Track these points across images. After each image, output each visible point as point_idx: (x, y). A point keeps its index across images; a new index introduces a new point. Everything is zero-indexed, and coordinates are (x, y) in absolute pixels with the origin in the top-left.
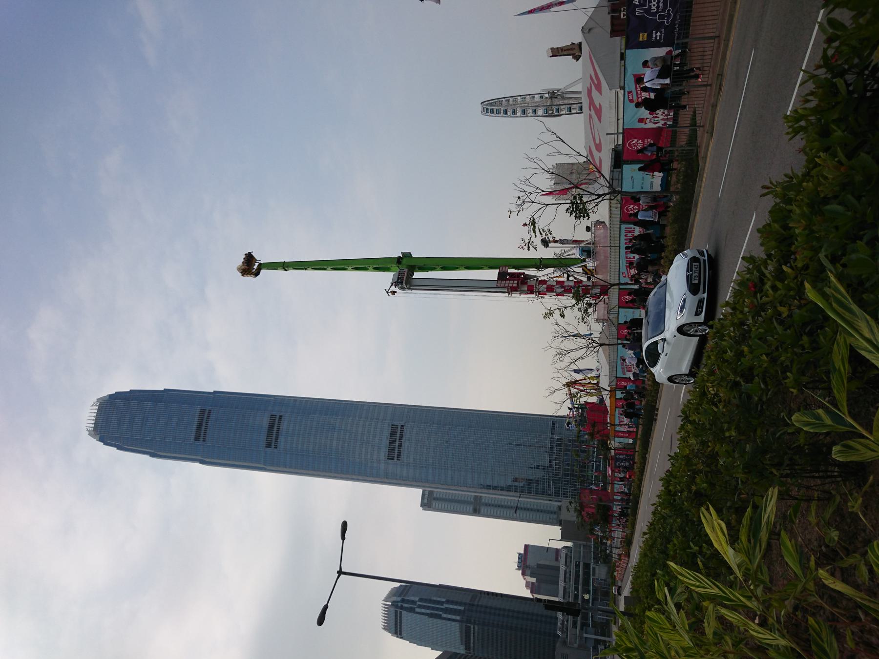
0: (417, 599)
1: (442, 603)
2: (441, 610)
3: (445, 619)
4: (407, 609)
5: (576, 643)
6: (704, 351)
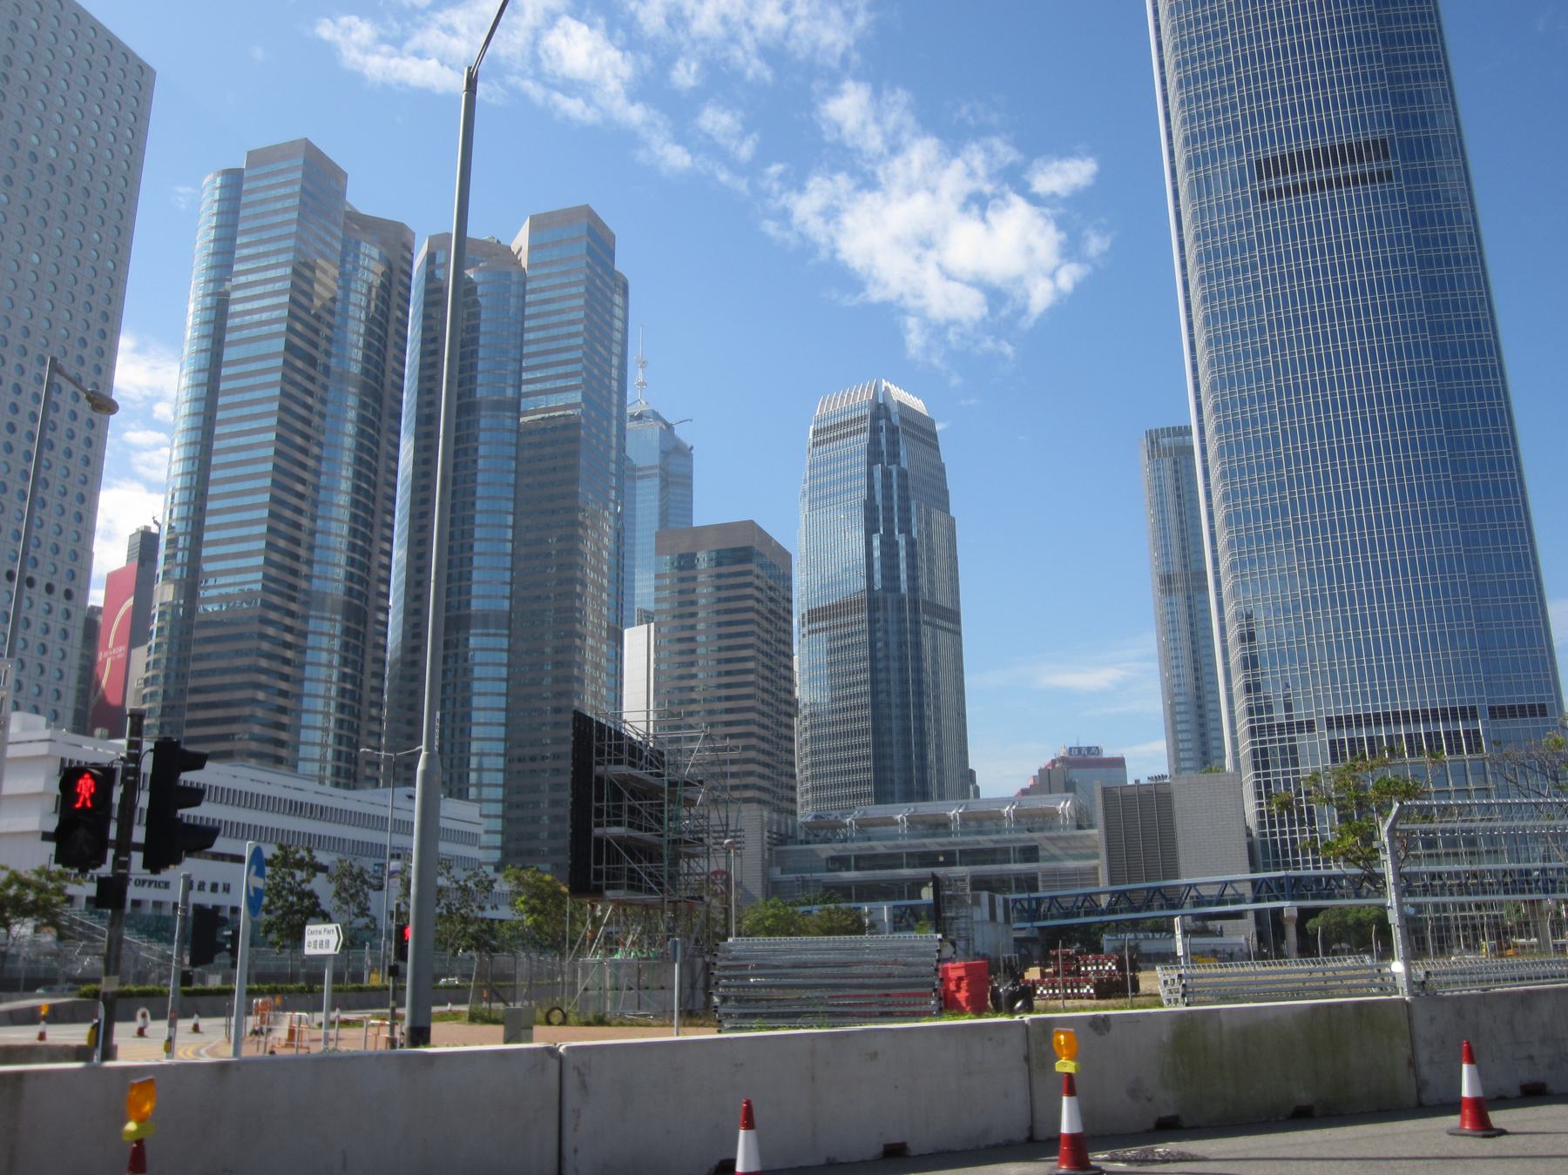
0: (904, 464)
1: (906, 529)
2: (889, 532)
3: (869, 544)
4: (874, 442)
5: (783, 872)
6: (196, 1016)
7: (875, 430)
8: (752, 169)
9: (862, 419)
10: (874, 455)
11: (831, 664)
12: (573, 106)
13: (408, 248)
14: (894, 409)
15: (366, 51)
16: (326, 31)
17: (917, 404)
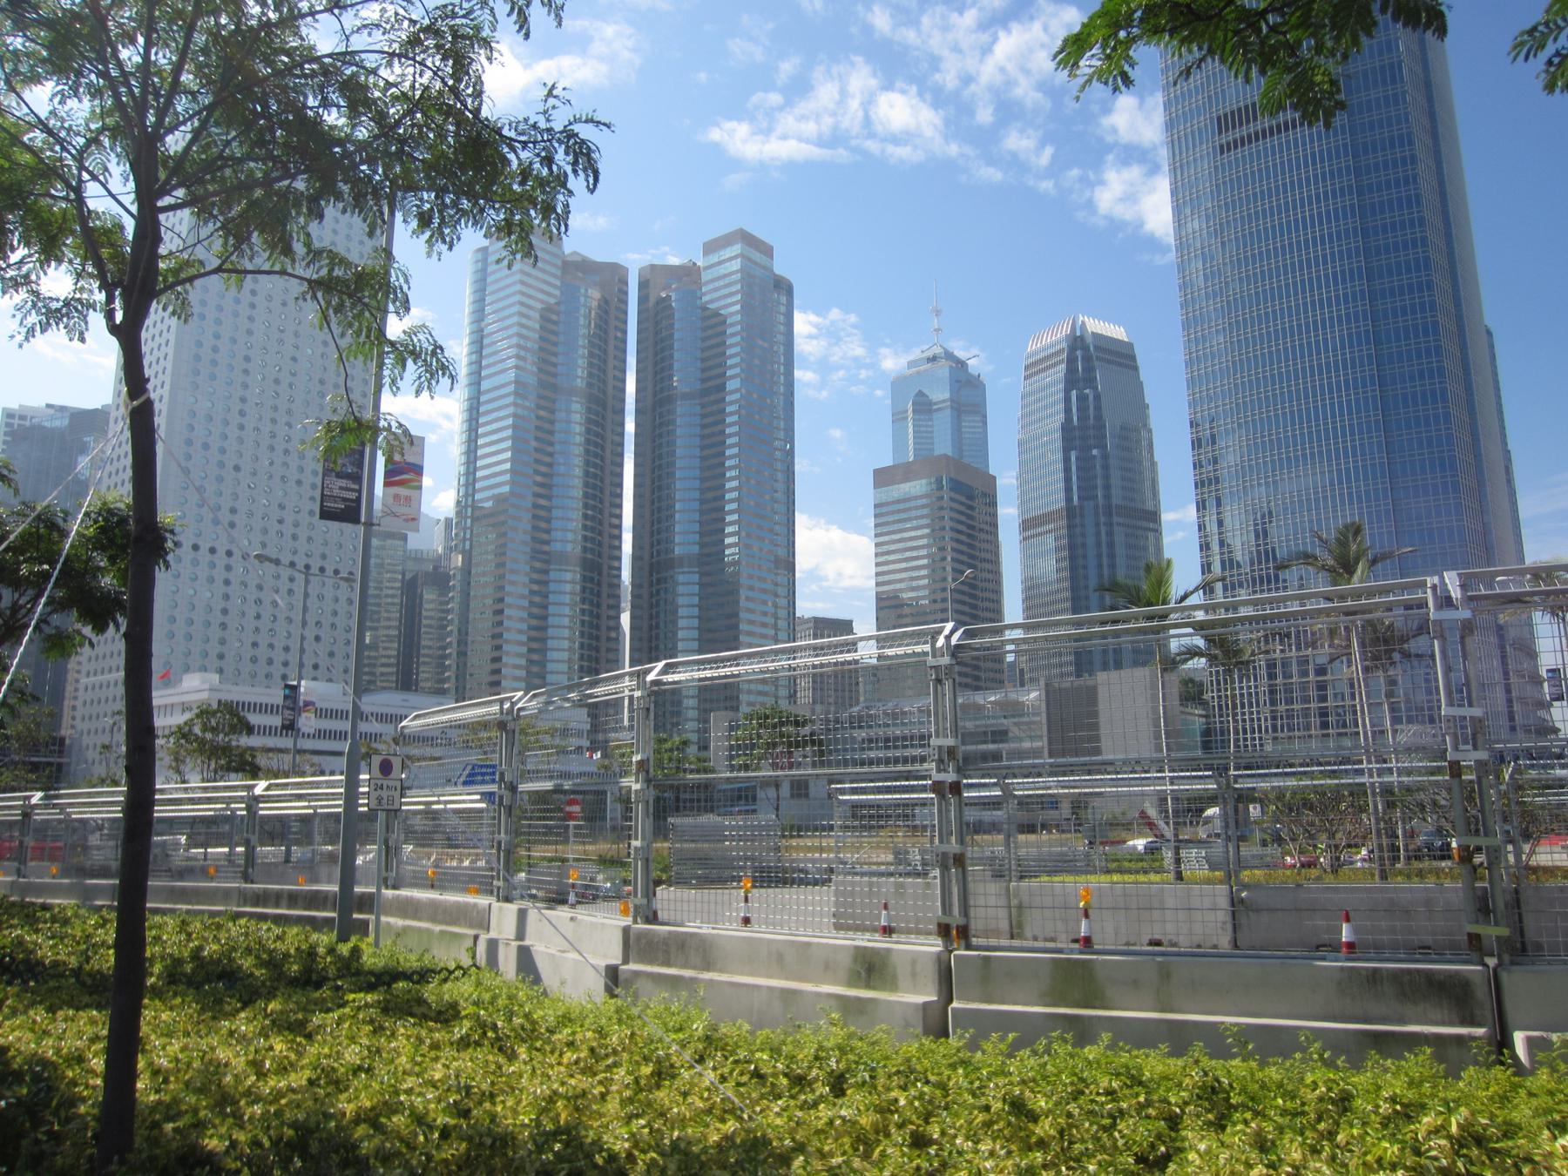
4: (1071, 369)
7: (1071, 361)
8: (1054, 170)
9: (1061, 351)
10: (1071, 381)
11: (877, 574)
12: (903, 152)
13: (625, 282)
14: (1089, 340)
15: (745, 141)
16: (715, 135)
17: (1117, 332)
